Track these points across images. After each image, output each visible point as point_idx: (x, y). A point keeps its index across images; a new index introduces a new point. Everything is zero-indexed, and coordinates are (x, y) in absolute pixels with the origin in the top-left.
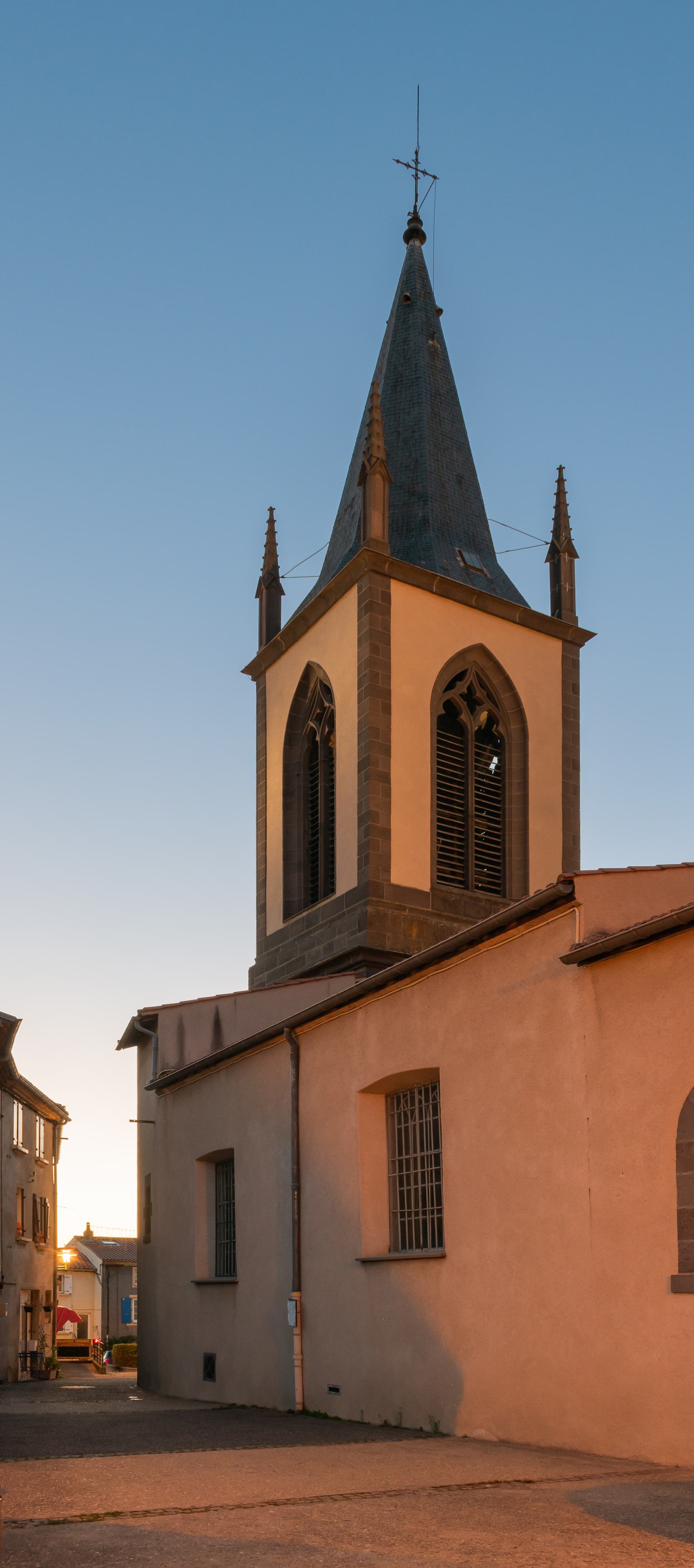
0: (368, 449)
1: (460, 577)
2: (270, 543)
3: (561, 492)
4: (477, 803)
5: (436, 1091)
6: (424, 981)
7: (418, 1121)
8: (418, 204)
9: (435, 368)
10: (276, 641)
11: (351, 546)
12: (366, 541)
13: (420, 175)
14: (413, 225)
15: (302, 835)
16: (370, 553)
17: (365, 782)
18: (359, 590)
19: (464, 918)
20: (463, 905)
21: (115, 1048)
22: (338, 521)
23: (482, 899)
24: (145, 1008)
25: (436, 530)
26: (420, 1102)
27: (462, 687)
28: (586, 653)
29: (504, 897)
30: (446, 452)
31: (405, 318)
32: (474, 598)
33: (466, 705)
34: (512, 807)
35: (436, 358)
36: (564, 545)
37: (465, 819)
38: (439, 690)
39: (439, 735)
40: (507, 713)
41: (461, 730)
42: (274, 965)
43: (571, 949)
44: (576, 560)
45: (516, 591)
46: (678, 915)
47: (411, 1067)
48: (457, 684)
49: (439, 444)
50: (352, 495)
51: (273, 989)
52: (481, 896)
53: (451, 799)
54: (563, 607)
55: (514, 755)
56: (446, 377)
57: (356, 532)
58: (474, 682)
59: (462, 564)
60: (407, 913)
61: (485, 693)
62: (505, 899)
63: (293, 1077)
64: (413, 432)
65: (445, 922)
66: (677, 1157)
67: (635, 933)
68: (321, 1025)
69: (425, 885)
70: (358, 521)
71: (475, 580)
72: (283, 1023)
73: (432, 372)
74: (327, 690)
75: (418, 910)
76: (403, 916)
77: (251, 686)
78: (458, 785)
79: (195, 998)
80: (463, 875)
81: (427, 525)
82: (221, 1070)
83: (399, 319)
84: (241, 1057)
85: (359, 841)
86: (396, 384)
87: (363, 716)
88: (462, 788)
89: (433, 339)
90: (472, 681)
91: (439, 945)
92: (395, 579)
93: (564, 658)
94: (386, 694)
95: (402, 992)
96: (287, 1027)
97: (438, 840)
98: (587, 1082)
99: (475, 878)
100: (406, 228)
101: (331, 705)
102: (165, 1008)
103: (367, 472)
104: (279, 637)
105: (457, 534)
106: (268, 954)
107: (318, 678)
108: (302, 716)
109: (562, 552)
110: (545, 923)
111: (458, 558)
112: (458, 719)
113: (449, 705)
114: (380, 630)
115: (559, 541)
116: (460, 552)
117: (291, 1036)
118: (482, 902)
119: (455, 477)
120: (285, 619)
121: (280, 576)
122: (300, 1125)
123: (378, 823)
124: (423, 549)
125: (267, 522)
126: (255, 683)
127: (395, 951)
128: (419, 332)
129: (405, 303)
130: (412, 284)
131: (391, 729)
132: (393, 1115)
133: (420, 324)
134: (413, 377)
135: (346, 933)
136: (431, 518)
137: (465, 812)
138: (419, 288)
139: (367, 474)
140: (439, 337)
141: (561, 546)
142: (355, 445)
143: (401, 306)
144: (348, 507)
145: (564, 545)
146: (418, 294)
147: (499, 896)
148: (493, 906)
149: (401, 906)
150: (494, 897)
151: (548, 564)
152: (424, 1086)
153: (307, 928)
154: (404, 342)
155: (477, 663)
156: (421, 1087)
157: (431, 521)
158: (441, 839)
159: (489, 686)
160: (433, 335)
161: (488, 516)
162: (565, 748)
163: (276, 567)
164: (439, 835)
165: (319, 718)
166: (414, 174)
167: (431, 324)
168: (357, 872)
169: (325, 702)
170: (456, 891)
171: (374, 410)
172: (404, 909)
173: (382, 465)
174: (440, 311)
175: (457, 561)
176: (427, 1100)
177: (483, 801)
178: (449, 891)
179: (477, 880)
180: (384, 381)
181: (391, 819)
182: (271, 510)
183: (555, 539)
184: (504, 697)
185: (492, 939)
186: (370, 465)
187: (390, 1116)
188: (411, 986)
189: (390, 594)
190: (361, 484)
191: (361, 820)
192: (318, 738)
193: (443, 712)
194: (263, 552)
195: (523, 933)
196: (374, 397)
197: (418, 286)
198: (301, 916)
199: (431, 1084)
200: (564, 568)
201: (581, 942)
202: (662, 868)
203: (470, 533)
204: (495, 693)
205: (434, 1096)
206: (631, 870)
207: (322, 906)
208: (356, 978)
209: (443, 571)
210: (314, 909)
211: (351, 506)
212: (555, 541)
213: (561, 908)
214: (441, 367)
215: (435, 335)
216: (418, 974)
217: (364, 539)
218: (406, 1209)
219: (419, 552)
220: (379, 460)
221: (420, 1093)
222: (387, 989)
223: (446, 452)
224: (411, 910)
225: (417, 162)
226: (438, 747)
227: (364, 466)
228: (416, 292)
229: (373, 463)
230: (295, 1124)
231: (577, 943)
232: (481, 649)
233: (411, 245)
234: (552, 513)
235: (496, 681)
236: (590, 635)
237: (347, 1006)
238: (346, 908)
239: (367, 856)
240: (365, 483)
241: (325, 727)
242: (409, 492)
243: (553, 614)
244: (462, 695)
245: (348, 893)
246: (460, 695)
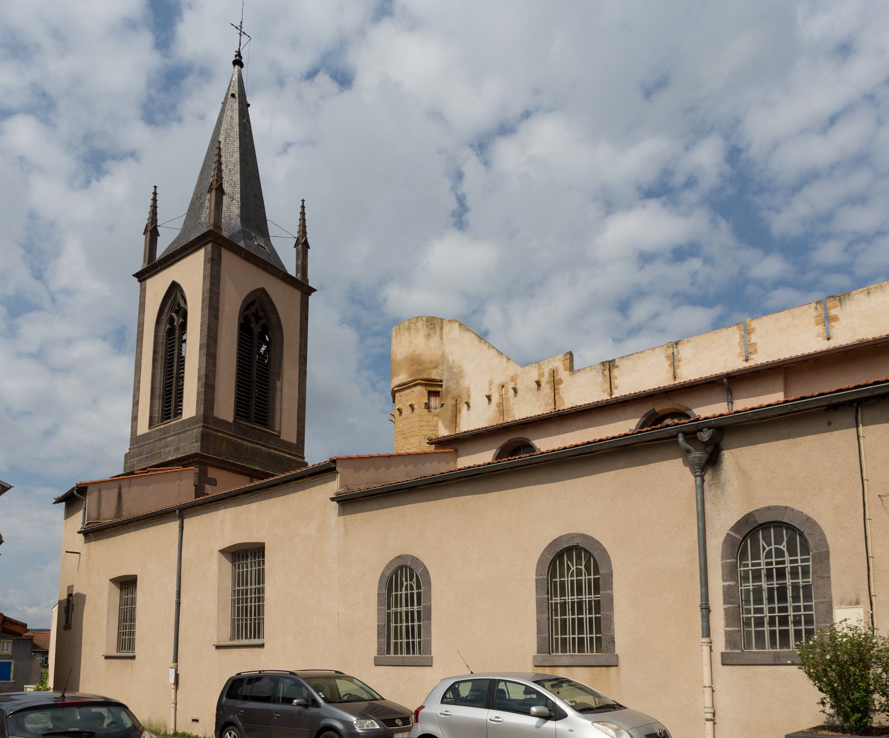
4: (257, 374)
13: (242, 34)
14: (237, 58)
18: (205, 250)
27: (253, 310)
28: (312, 299)
39: (240, 334)
42: (142, 454)
43: (334, 495)
44: (309, 250)
66: (378, 599)
85: (198, 390)
90: (257, 307)
92: (223, 247)
93: (302, 300)
95: (246, 500)
121: (158, 225)
153: (164, 435)
162: (300, 349)
163: (156, 220)
174: (249, 105)
179: (256, 417)
193: (243, 322)
213: (330, 473)
218: (244, 617)
222: (238, 497)
244: (253, 314)
245: (190, 419)
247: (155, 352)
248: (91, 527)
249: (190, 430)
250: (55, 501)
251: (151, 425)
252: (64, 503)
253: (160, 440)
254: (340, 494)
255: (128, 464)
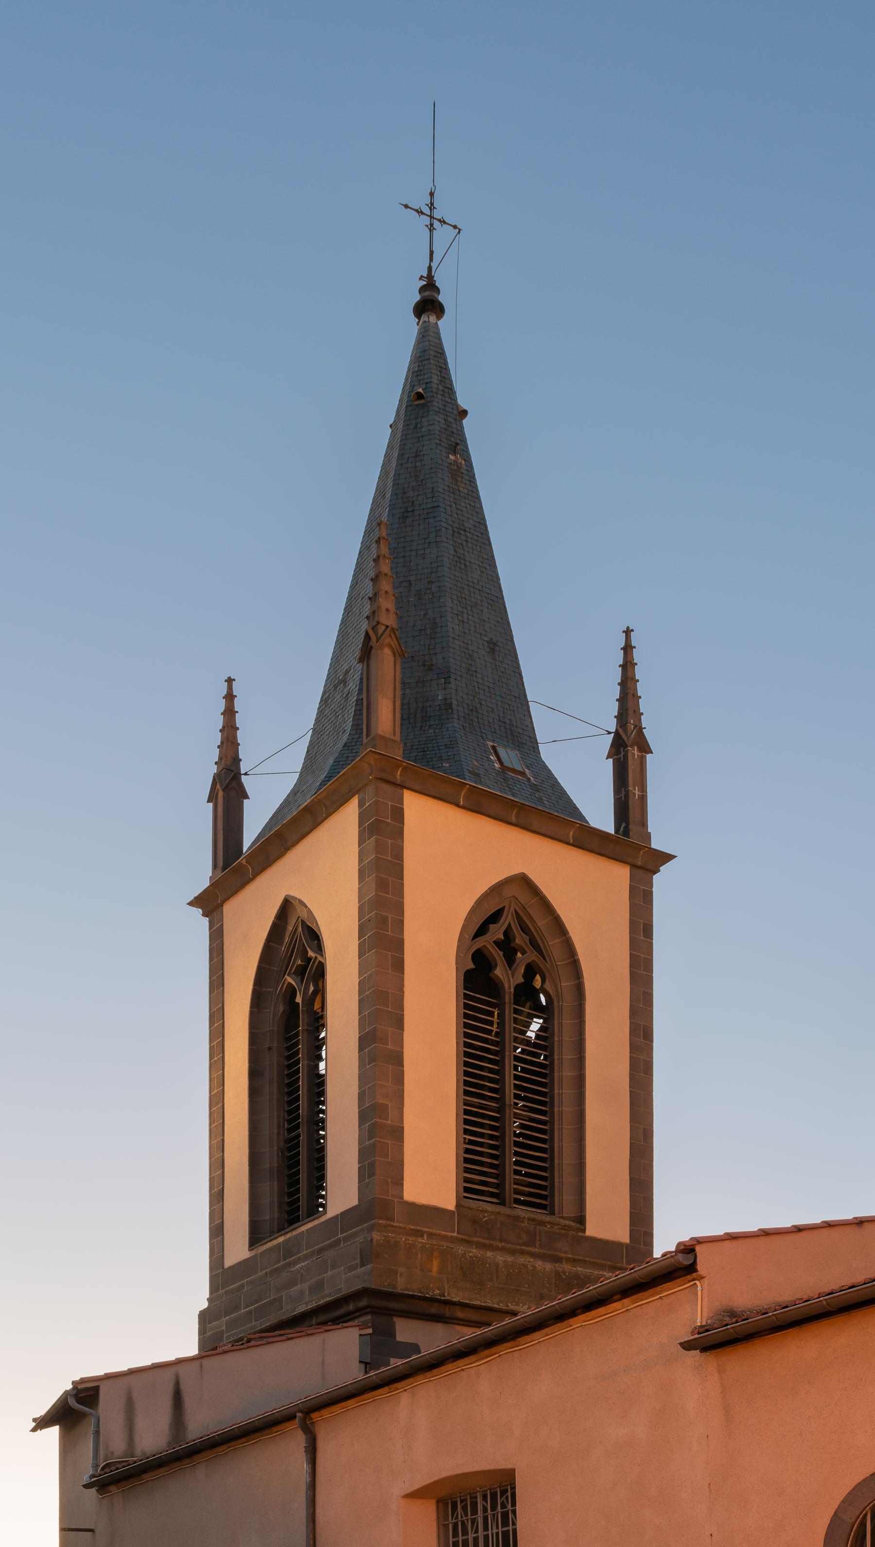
0: (374, 612)
1: (495, 784)
2: (228, 726)
3: (628, 664)
5: (505, 1495)
6: (491, 1362)
7: (481, 1533)
8: (434, 265)
9: (458, 492)
10: (240, 866)
11: (345, 738)
12: (370, 737)
13: (436, 224)
14: (427, 293)
15: (276, 1131)
16: (377, 756)
17: (368, 1065)
18: (361, 804)
19: (500, 1245)
20: (499, 1226)
21: (30, 1429)
22: (325, 701)
23: (524, 1218)
24: (82, 1379)
25: (462, 719)
26: (485, 1510)
27: (496, 932)
29: (552, 1213)
30: (475, 610)
31: (417, 424)
32: (514, 812)
33: (502, 956)
34: (563, 1093)
35: (460, 479)
36: (633, 736)
37: (501, 1110)
38: (468, 937)
39: (466, 996)
40: (556, 965)
41: (493, 988)
42: (237, 1308)
43: (693, 1333)
44: (648, 756)
45: (569, 801)
46: (827, 1300)
47: (476, 1468)
48: (491, 928)
49: (465, 599)
50: (346, 667)
51: (251, 1348)
52: (522, 1214)
53: (482, 1083)
54: (631, 821)
55: (565, 1023)
56: (473, 505)
57: (351, 719)
58: (511, 923)
59: (497, 765)
60: (425, 1239)
61: (527, 938)
62: (554, 1217)
63: (308, 1476)
64: (430, 582)
65: (475, 1251)
67: (775, 1320)
68: (348, 1409)
69: (449, 1202)
70: (354, 703)
71: (515, 788)
72: (296, 1406)
73: (455, 499)
74: (314, 936)
75: (439, 1235)
76: (420, 1245)
77: (200, 923)
78: (489, 1064)
79: (147, 1363)
80: (497, 1186)
81: (450, 711)
82: (198, 1463)
83: (408, 425)
84: (229, 1447)
85: (360, 1144)
86: (405, 514)
87: (366, 975)
88: (497, 1068)
89: (455, 453)
90: (509, 924)
91: (519, 1319)
93: (632, 889)
94: (399, 945)
95: (464, 1373)
96: (301, 1411)
97: (465, 1138)
98: (710, 1491)
99: (514, 1188)
100: (417, 297)
101: (318, 956)
102: (109, 1377)
103: (371, 644)
104: (244, 860)
105: (489, 722)
106: (227, 1293)
107: (299, 917)
108: (276, 969)
109: (630, 747)
110: (658, 1297)
111: (492, 757)
112: (491, 975)
113: (479, 957)
114: (390, 858)
115: (626, 732)
116: (494, 748)
117: (306, 1422)
118: (523, 1222)
119: (486, 644)
120: (250, 836)
121: (242, 772)
122: (317, 1538)
123: (388, 1120)
124: (446, 745)
125: (224, 698)
126: (208, 919)
127: (411, 1293)
128: (437, 444)
129: (417, 403)
130: (426, 376)
131: (403, 992)
132: (446, 1526)
133: (437, 432)
134: (429, 506)
135: (342, 1268)
136: (455, 702)
137: (501, 1101)
138: (436, 381)
139: (371, 647)
140: (463, 450)
141: (628, 738)
142: (346, 595)
143: (411, 406)
144: (340, 682)
145: (633, 736)
146: (434, 390)
147: (546, 1212)
148: (538, 1227)
149: (417, 1230)
150: (539, 1214)
151: (611, 760)
152: (490, 1489)
153: (285, 1259)
154: (416, 456)
155: (517, 899)
156: (486, 1491)
157: (454, 706)
158: (468, 1137)
159: (533, 930)
160: (455, 447)
161: (529, 698)
163: (237, 760)
164: (466, 1131)
165: (301, 972)
166: (428, 223)
167: (453, 432)
168: (357, 1185)
169: (309, 950)
170: (489, 1207)
171: (381, 558)
172: (421, 1234)
173: (392, 635)
175: (489, 760)
176: (494, 1508)
177: (524, 1084)
178: (480, 1209)
179: (517, 1192)
180: (389, 510)
181: (404, 1114)
182: (230, 681)
183: (621, 727)
184: (553, 944)
185: (587, 1313)
186: (377, 636)
187: (442, 1526)
188: (476, 1366)
189: (402, 810)
190: (364, 660)
191: (363, 1116)
192: (299, 999)
193: (472, 966)
194: (217, 738)
195: (628, 1308)
196: (382, 544)
197: (435, 379)
198: (275, 1242)
199: (500, 1487)
200: (632, 766)
201: (704, 1323)
202: (798, 1229)
203: (508, 722)
204: (542, 940)
205: (503, 1501)
206: (762, 1233)
207: (307, 1230)
208: (360, 1329)
209: (473, 776)
210: (294, 1233)
211: (344, 682)
212: (620, 731)
213: (678, 1281)
214: (466, 491)
215: (458, 447)
216: (487, 1352)
217: (367, 736)
219: (439, 749)
220: (389, 628)
221: (485, 1498)
222: (443, 1368)
223: (475, 610)
224: (430, 1235)
225: (432, 206)
226: (465, 1013)
227: (367, 636)
228: (432, 387)
229: (380, 633)
230: (311, 1536)
231: (699, 1324)
232: (523, 881)
233: (425, 322)
234: (616, 692)
235: (542, 922)
236: (667, 858)
237: (386, 1387)
238: (342, 1233)
239: (372, 1165)
240: (369, 658)
241: (310, 984)
242: (424, 665)
243: (617, 830)
244: (497, 943)
246: (494, 942)
247: (254, 1074)
248: (111, 1471)
249: (346, 1239)
250: (34, 1424)
251: (255, 1240)
252: (54, 1431)
253: (276, 1270)
254: (708, 1331)
255: (209, 1334)
